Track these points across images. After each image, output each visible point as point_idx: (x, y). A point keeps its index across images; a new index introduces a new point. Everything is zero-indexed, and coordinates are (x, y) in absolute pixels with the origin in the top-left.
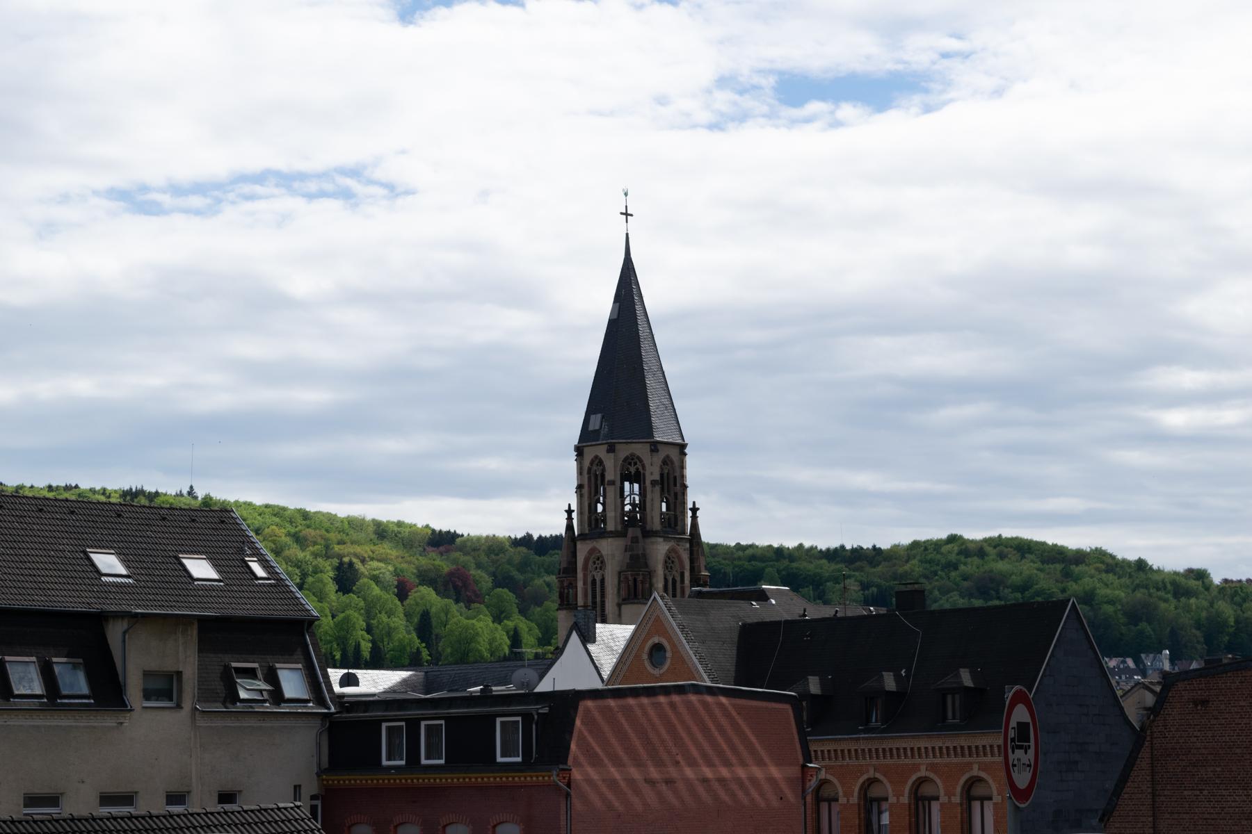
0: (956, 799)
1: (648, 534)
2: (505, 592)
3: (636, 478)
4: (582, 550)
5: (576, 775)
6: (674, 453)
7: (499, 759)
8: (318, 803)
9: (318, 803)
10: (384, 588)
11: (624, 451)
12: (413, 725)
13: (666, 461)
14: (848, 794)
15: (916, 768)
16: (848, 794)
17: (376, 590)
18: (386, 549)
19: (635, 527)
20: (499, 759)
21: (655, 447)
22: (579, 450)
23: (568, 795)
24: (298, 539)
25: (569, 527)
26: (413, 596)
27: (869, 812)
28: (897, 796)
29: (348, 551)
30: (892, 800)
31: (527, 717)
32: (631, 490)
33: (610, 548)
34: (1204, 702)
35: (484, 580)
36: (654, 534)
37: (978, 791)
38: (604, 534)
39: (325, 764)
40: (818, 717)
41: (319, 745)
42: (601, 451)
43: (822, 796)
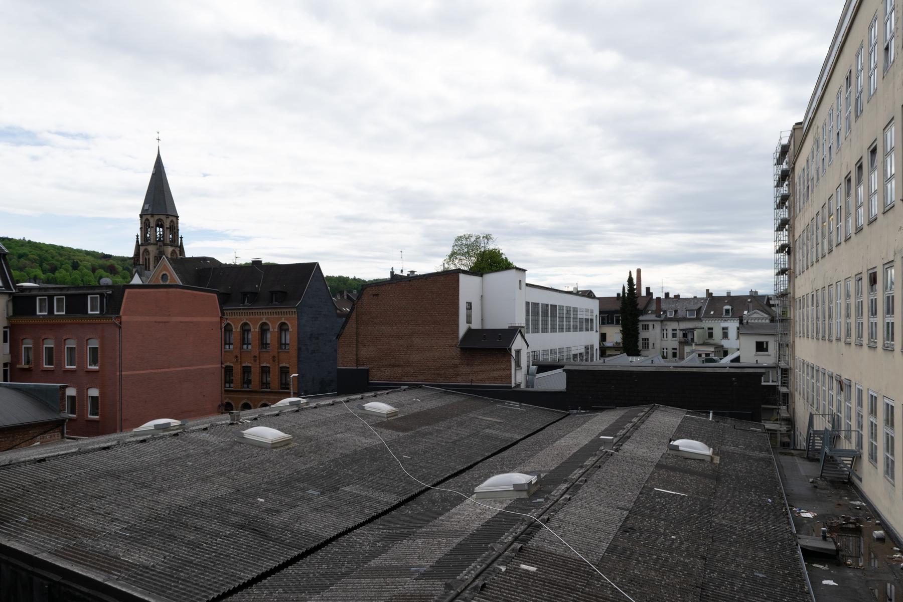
0: (276, 330)
1: (165, 245)
2: (126, 272)
3: (161, 226)
4: (142, 249)
5: (124, 318)
6: (174, 219)
7: (90, 312)
8: (8, 330)
9: (8, 330)
10: (87, 269)
11: (156, 217)
12: (51, 298)
13: (172, 221)
14: (236, 328)
15: (261, 319)
16: (236, 328)
17: (85, 270)
18: (89, 258)
19: (161, 243)
20: (90, 312)
21: (168, 216)
22: (141, 216)
23: (120, 328)
24: (61, 255)
25: (137, 241)
26: (97, 271)
27: (244, 334)
28: (255, 329)
29: (76, 259)
30: (271, 330)
31: (102, 295)
32: (159, 231)
33: (151, 248)
34: (377, 295)
35: (120, 268)
36: (167, 245)
37: (284, 327)
38: (149, 244)
39: (11, 313)
40: (225, 299)
41: (7, 306)
42: (149, 217)
43: (228, 329)
